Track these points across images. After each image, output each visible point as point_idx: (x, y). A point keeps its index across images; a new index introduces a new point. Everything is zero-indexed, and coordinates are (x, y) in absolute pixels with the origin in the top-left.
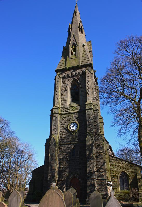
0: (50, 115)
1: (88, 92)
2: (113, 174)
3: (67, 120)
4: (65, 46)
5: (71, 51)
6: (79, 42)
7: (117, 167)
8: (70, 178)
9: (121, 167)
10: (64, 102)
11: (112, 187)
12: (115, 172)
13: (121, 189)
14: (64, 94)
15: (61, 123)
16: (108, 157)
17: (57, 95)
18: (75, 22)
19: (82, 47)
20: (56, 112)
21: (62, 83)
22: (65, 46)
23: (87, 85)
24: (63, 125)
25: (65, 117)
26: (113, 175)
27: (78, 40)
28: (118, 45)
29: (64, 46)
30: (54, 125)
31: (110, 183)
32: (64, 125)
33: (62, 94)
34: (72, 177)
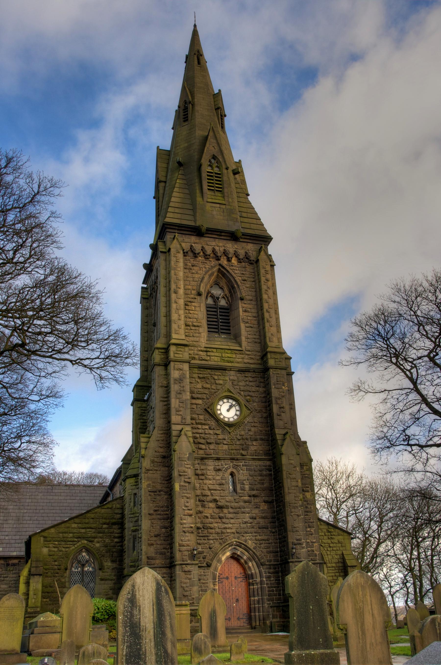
1: (270, 319)
3: (208, 386)
4: (167, 145)
10: (193, 328)
14: (193, 304)
15: (192, 392)
22: (167, 145)
23: (265, 297)
24: (198, 398)
25: (204, 378)
30: (176, 398)
32: (200, 402)
33: (186, 305)
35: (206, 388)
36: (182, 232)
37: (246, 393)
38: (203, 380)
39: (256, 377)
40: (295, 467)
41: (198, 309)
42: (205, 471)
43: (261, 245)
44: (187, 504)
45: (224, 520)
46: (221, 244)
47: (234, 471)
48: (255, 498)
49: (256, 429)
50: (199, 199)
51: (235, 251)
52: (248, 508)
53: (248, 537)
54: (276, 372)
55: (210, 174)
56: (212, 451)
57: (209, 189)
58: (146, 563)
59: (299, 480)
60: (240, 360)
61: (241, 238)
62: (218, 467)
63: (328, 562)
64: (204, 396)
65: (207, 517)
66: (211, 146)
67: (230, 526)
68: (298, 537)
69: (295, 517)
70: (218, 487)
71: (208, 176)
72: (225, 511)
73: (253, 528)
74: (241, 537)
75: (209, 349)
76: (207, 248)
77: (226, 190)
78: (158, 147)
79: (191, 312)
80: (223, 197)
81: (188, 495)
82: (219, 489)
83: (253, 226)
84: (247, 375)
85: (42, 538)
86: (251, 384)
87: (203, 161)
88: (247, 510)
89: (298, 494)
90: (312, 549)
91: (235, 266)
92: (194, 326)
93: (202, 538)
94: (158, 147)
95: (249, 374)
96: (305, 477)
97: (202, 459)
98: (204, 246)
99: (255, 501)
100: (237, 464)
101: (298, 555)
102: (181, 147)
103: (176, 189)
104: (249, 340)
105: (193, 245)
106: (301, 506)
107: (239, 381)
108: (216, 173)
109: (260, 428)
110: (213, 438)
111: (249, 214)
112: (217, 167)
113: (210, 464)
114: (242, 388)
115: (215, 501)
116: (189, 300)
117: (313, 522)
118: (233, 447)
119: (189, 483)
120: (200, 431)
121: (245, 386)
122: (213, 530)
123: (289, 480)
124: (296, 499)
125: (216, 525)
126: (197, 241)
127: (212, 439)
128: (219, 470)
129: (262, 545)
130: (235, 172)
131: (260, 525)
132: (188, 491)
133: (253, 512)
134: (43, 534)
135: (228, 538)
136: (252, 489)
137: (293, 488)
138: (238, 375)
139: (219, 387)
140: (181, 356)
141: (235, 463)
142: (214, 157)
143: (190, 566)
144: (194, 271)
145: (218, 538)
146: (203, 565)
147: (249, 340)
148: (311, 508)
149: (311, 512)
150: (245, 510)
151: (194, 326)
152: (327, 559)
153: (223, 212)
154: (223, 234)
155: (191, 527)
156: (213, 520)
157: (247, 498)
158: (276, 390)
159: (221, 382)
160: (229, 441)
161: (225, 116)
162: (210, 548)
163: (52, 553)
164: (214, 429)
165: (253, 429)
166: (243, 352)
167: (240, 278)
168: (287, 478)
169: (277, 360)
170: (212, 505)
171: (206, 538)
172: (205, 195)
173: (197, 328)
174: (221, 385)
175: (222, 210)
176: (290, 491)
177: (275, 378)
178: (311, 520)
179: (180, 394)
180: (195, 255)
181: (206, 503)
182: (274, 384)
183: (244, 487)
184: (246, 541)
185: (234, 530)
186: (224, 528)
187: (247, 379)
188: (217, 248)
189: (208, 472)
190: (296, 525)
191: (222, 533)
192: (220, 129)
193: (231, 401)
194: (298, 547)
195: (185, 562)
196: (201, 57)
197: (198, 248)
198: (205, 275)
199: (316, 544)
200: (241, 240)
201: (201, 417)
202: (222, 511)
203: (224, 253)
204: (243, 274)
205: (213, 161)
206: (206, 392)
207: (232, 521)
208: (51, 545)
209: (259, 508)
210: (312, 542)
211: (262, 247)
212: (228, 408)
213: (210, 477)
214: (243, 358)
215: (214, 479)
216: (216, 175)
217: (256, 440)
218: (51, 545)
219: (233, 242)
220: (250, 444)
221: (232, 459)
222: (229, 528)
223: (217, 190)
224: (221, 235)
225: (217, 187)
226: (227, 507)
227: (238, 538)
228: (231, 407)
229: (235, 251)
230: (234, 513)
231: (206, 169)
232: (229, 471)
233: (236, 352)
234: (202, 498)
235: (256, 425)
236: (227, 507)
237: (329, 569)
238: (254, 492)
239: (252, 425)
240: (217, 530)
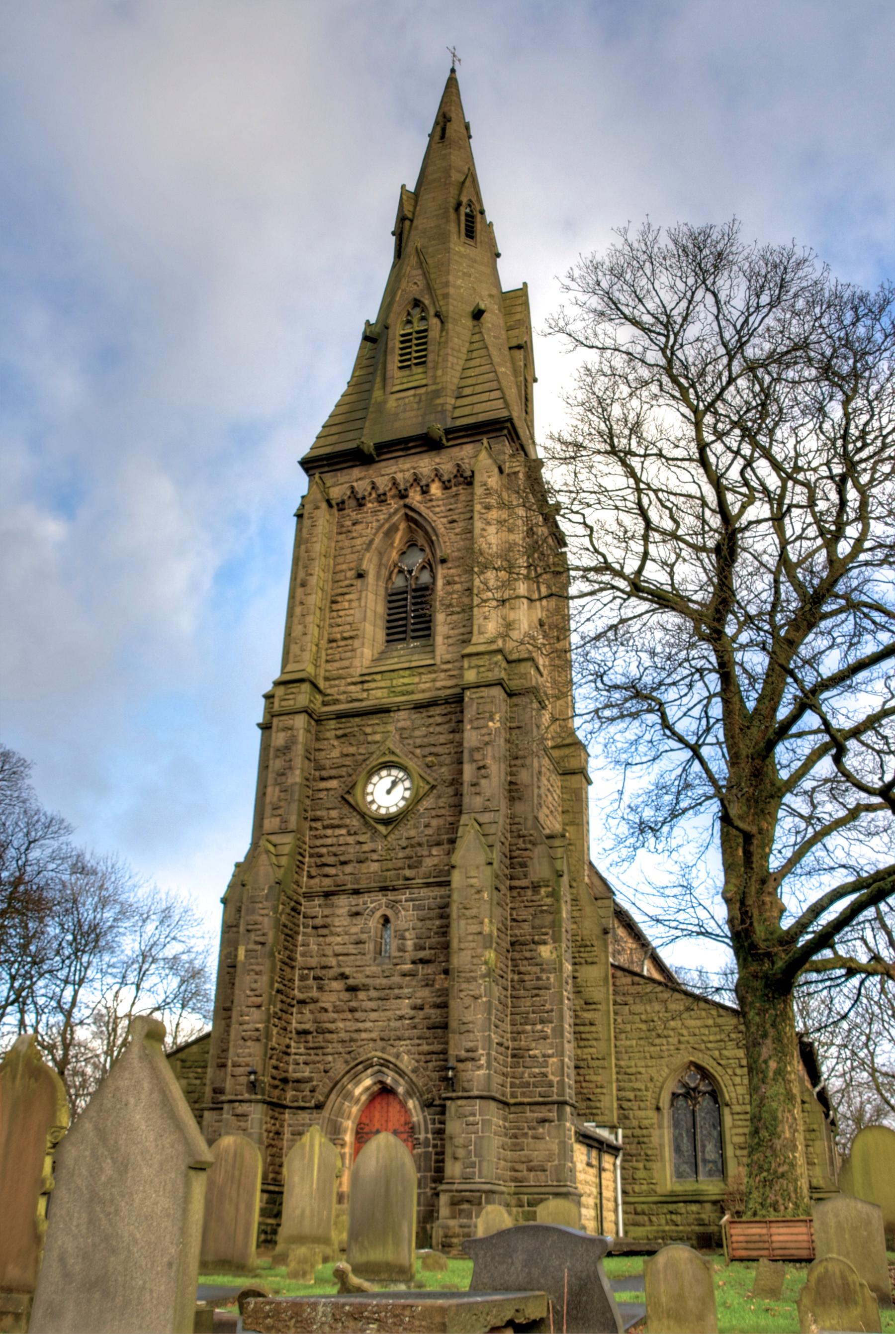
0: (259, 725)
2: (630, 1081)
3: (352, 750)
4: (373, 321)
5: (402, 349)
6: (452, 291)
7: (659, 1036)
8: (357, 1091)
9: (680, 1042)
10: (342, 643)
11: (623, 1161)
12: (643, 1070)
13: (679, 1175)
14: (347, 597)
16: (606, 979)
17: (302, 603)
18: (436, 176)
19: (468, 322)
20: (291, 702)
21: (340, 537)
22: (373, 321)
24: (331, 778)
25: (345, 735)
26: (634, 1090)
27: (447, 284)
28: (573, 285)
29: (368, 321)
30: (276, 784)
31: (612, 1138)
32: (333, 784)
34: (367, 1089)
35: (347, 755)
37: (427, 750)
38: (342, 740)
39: (450, 713)
40: (479, 892)
41: (355, 604)
42: (329, 920)
44: (254, 986)
45: (358, 1015)
46: (407, 466)
47: (389, 913)
48: (425, 966)
49: (441, 821)
50: (377, 394)
52: (408, 986)
53: (403, 1047)
54: (477, 695)
55: (406, 339)
56: (349, 878)
57: (401, 368)
58: (210, 1099)
59: (486, 921)
60: (428, 685)
61: (448, 440)
62: (354, 909)
63: (734, 1101)
64: (343, 771)
65: (326, 1010)
67: (368, 1025)
68: (470, 1045)
69: (468, 1001)
70: (352, 949)
72: (362, 995)
73: (415, 1027)
74: (389, 1048)
75: (367, 678)
79: (341, 613)
81: (257, 968)
82: (354, 952)
84: (431, 713)
85: (179, 1063)
86: (438, 729)
88: (406, 991)
89: (479, 951)
90: (543, 1070)
91: (438, 500)
92: (345, 639)
93: (312, 1052)
95: (437, 710)
96: (542, 912)
97: (327, 895)
99: (425, 972)
100: (392, 898)
101: (466, 1085)
104: (451, 641)
105: (355, 484)
106: (483, 976)
107: (414, 729)
109: (449, 819)
110: (352, 851)
113: (341, 904)
114: (419, 741)
115: (343, 976)
116: (340, 591)
117: (552, 1011)
118: (390, 865)
119: (263, 944)
120: (329, 841)
121: (425, 736)
122: (334, 1036)
123: (463, 922)
124: (475, 961)
125: (341, 1025)
126: (363, 474)
127: (352, 852)
128: (357, 914)
129: (430, 1065)
131: (431, 1021)
132: (260, 960)
133: (418, 995)
134: (179, 1055)
135: (361, 1050)
136: (419, 948)
137: (470, 938)
138: (414, 716)
139: (373, 748)
140: (291, 702)
141: (391, 896)
142: (417, 303)
143: (248, 1104)
144: (354, 534)
145: (341, 1050)
146: (307, 1105)
147: (451, 641)
148: (548, 979)
149: (546, 988)
150: (401, 991)
151: (345, 639)
152: (733, 1095)
154: (411, 445)
155: (257, 1030)
156: (335, 1015)
157: (408, 967)
158: (474, 733)
159: (377, 737)
160: (384, 853)
162: (326, 1072)
163: (192, 1088)
164: (355, 833)
165: (434, 822)
166: (435, 668)
167: (444, 520)
168: (459, 917)
169: (482, 669)
170: (337, 985)
171: (320, 1052)
173: (350, 642)
174: (378, 742)
175: (417, 399)
176: (462, 946)
177: (475, 706)
178: (548, 1007)
179: (283, 774)
180: (360, 503)
181: (326, 982)
182: (471, 721)
183: (403, 944)
184: (397, 1056)
185: (374, 1035)
186: (356, 1031)
187: (431, 720)
188: (399, 476)
189: (337, 919)
190: (468, 1018)
191: (352, 1040)
193: (394, 772)
194: (469, 1065)
195: (240, 1098)
197: (362, 487)
198: (375, 535)
199: (555, 1060)
201: (334, 813)
202: (356, 996)
204: (450, 510)
206: (348, 763)
207: (374, 1016)
208: (191, 1075)
209: (432, 986)
210: (544, 1056)
212: (389, 785)
213: (338, 930)
214: (434, 680)
215: (346, 934)
217: (438, 844)
218: (191, 1075)
220: (425, 853)
221: (384, 889)
222: (365, 1031)
223: (416, 364)
226: (366, 988)
227: (383, 1050)
228: (394, 784)
229: (436, 470)
230: (379, 999)
232: (378, 914)
233: (421, 670)
234: (319, 973)
235: (442, 812)
236: (366, 988)
237: (736, 1117)
238: (422, 954)
239: (434, 813)
240: (343, 1035)
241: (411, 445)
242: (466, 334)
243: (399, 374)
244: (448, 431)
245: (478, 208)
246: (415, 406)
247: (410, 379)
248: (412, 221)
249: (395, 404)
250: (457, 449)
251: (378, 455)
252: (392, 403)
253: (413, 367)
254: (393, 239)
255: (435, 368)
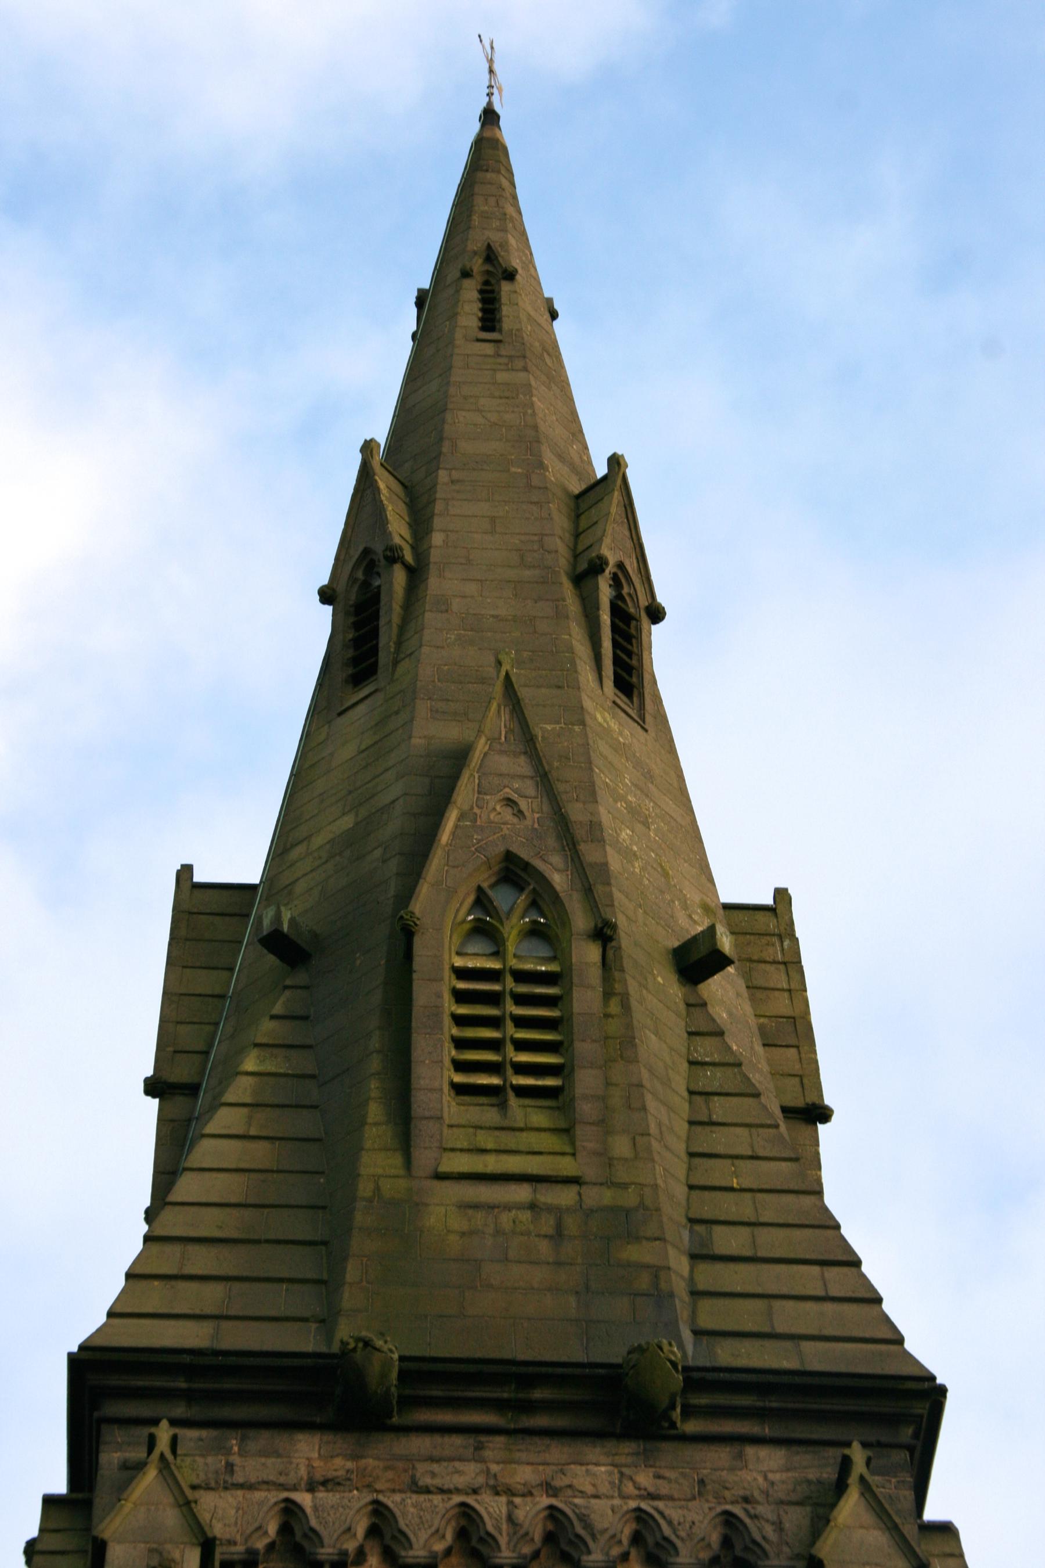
36: (227, 1412)
43: (834, 1454)
46: (524, 1474)
50: (377, 1164)
51: (640, 1516)
55: (476, 990)
57: (460, 1090)
61: (688, 1412)
66: (492, 800)
71: (461, 997)
76: (407, 1509)
77: (586, 1081)
78: (185, 872)
80: (567, 1132)
83: (789, 1317)
87: (423, 902)
94: (185, 872)
98: (391, 1501)
102: (318, 841)
103: (224, 1120)
105: (304, 1499)
108: (521, 976)
111: (765, 1235)
112: (535, 932)
126: (340, 1466)
130: (696, 955)
142: (513, 871)
153: (558, 1236)
154: (537, 1394)
161: (656, 614)
172: (424, 1132)
175: (547, 1225)
188: (492, 1509)
192: (597, 697)
196: (505, 287)
200: (692, 1427)
203: (549, 1538)
205: (503, 898)
211: (846, 1464)
216: (523, 989)
219: (628, 1447)
223: (522, 1092)
224: (528, 1407)
225: (522, 1069)
229: (640, 1516)
231: (445, 950)
241: (537, 1394)
242: (675, 1025)
243: (452, 1108)
244: (698, 1379)
245: (643, 602)
246: (544, 1248)
247: (509, 1140)
248: (416, 574)
249: (457, 1222)
250: (721, 1455)
251: (408, 1402)
252: (443, 1211)
253: (513, 1101)
254: (321, 620)
255: (604, 1124)
